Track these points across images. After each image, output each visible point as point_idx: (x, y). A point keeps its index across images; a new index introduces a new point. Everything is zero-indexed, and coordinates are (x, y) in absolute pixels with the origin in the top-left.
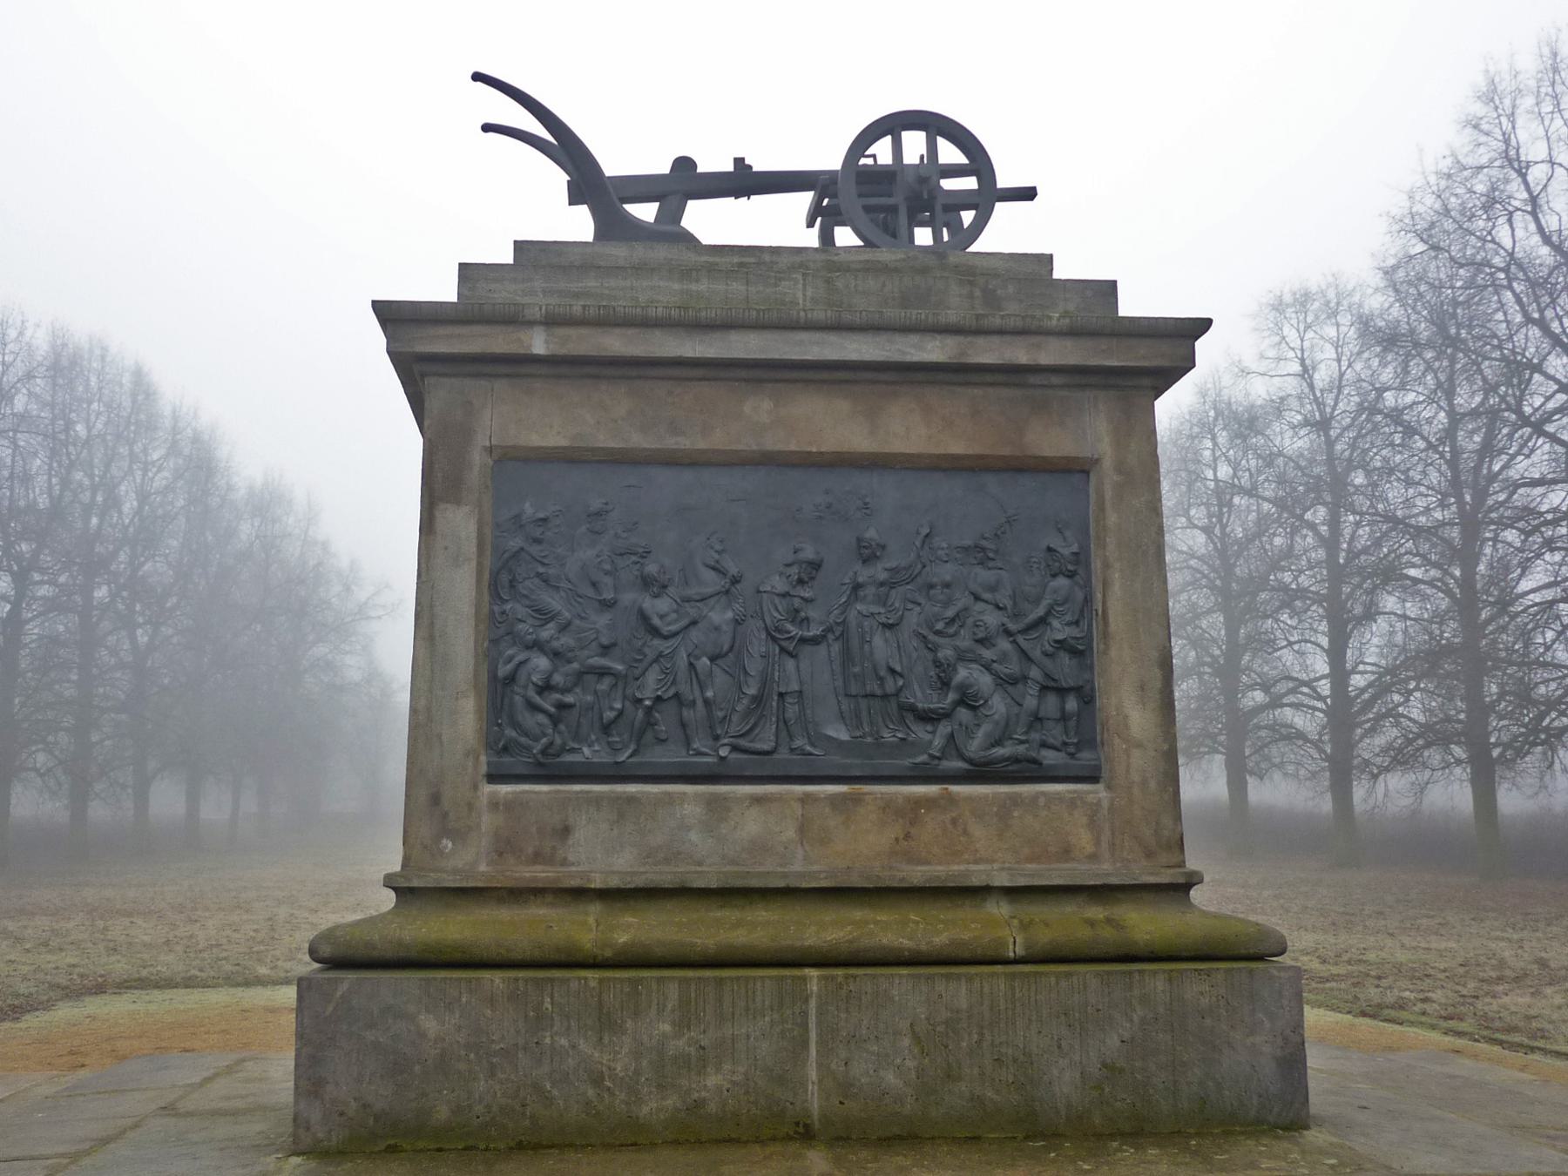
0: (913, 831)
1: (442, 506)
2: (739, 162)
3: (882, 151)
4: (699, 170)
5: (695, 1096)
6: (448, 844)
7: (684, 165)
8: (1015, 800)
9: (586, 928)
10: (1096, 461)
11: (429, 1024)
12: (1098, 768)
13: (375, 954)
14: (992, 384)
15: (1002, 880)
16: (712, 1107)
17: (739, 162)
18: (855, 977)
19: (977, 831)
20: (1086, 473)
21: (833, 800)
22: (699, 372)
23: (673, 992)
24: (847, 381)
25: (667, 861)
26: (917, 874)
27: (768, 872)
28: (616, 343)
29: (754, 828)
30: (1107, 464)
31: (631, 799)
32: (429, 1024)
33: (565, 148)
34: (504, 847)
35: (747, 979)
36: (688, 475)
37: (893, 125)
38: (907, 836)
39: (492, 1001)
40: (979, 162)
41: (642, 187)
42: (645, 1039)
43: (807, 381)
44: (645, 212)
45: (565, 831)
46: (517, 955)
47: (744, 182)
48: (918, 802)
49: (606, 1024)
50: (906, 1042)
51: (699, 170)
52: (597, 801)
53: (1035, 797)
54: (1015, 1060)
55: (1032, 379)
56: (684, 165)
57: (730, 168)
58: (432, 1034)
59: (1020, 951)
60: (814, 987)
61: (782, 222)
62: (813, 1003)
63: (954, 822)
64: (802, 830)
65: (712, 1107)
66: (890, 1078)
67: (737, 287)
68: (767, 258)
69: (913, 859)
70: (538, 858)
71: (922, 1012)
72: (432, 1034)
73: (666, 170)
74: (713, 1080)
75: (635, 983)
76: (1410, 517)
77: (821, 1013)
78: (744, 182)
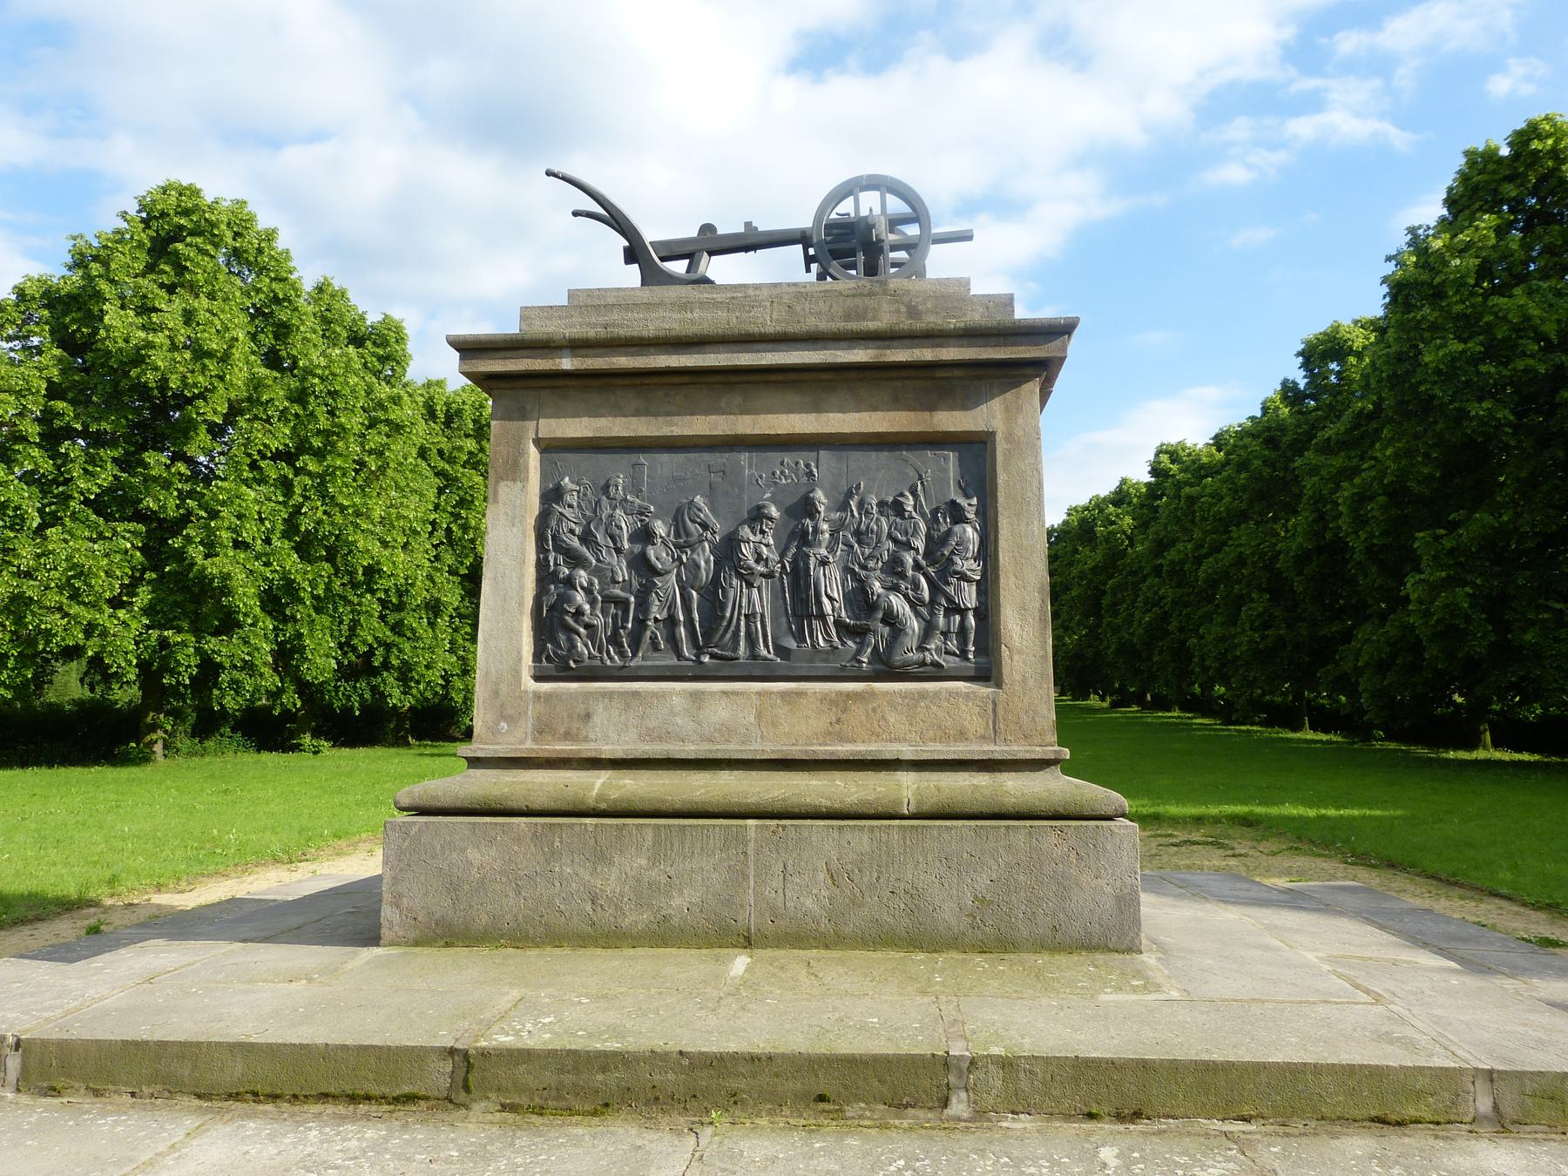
0: (843, 717)
1: (502, 484)
2: (748, 224)
3: (846, 207)
4: (719, 232)
5: (663, 912)
6: (504, 725)
7: (707, 229)
8: (923, 695)
9: (597, 785)
10: (992, 434)
11: (473, 855)
12: (990, 670)
13: (439, 804)
14: (908, 378)
15: (907, 752)
16: (675, 921)
17: (748, 224)
18: (784, 827)
19: (892, 718)
20: (985, 443)
21: (784, 695)
22: (686, 379)
23: (649, 835)
24: (673, 385)
25: (660, 738)
26: (843, 750)
27: (732, 749)
28: (623, 362)
29: (725, 712)
30: (999, 437)
31: (636, 694)
32: (473, 855)
33: (616, 220)
34: (542, 729)
35: (703, 826)
36: (679, 457)
37: (849, 189)
38: (838, 721)
39: (518, 840)
40: (918, 214)
41: (673, 251)
42: (628, 869)
43: (624, 386)
44: (679, 267)
45: (588, 716)
46: (536, 806)
47: (750, 242)
48: (849, 696)
49: (601, 858)
50: (822, 876)
51: (719, 232)
52: (610, 695)
53: (937, 694)
54: (906, 893)
55: (940, 374)
56: (707, 229)
57: (742, 230)
58: (476, 863)
59: (913, 808)
60: (752, 834)
61: (787, 266)
62: (752, 845)
63: (874, 710)
64: (759, 716)
65: (675, 921)
66: (809, 903)
67: (722, 315)
68: (751, 292)
69: (842, 739)
70: (568, 736)
71: (834, 855)
72: (476, 863)
73: (694, 233)
74: (677, 901)
75: (620, 828)
76: (91, 540)
77: (758, 852)
78: (750, 242)
